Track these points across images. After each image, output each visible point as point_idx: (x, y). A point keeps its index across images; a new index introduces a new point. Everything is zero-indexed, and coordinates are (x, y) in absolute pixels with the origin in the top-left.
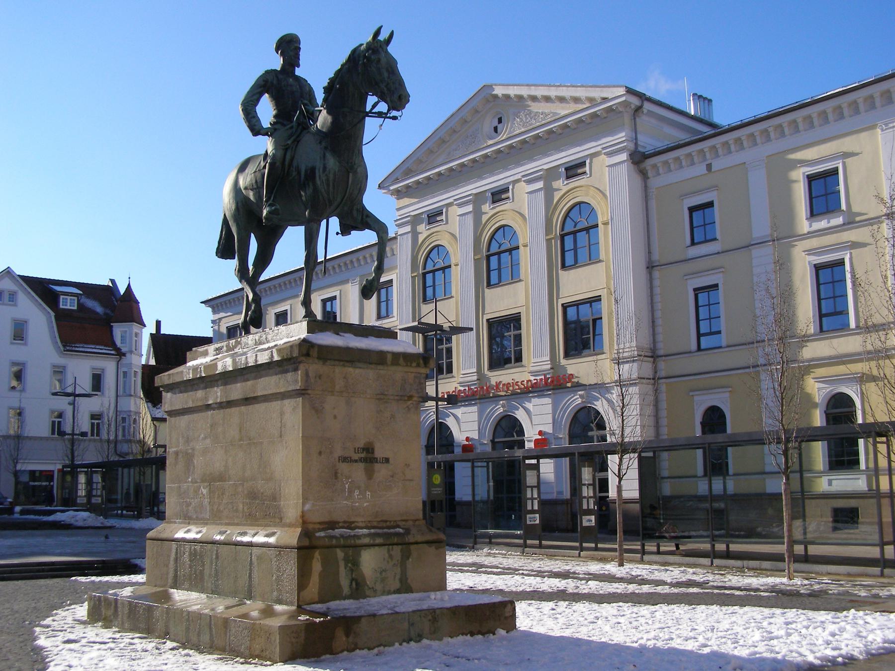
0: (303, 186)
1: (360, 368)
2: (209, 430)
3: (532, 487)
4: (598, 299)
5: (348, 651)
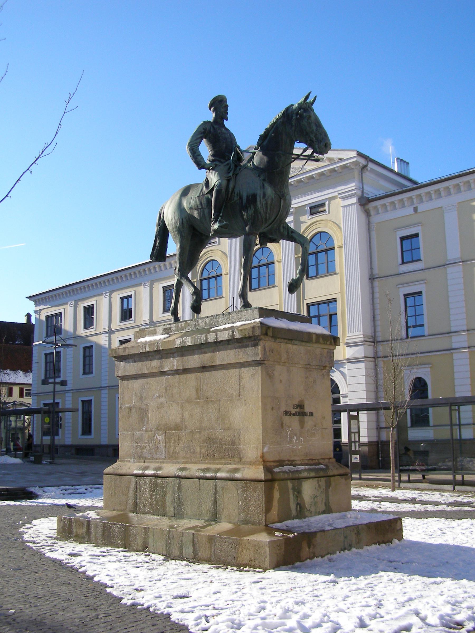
0: (245, 208)
1: (296, 345)
2: (164, 391)
3: (355, 433)
4: (334, 300)
5: (310, 559)
